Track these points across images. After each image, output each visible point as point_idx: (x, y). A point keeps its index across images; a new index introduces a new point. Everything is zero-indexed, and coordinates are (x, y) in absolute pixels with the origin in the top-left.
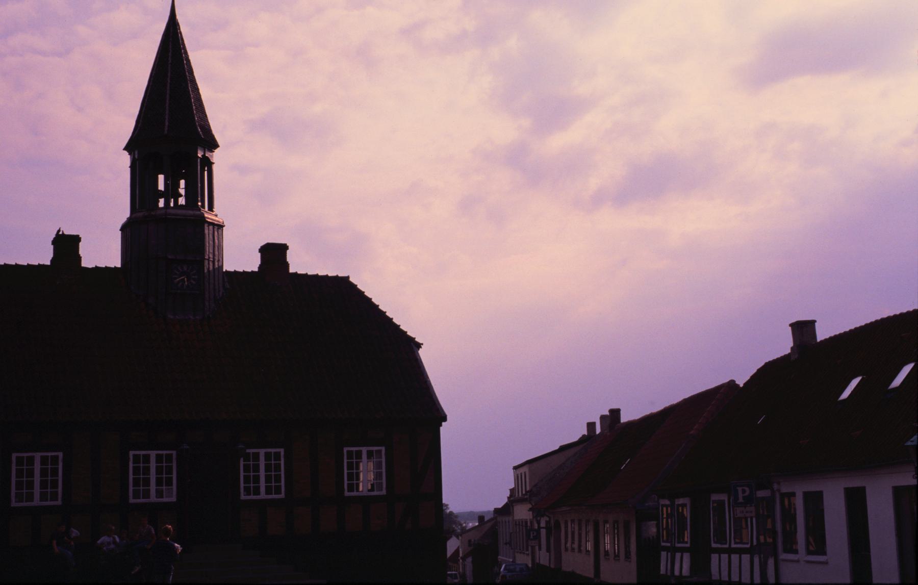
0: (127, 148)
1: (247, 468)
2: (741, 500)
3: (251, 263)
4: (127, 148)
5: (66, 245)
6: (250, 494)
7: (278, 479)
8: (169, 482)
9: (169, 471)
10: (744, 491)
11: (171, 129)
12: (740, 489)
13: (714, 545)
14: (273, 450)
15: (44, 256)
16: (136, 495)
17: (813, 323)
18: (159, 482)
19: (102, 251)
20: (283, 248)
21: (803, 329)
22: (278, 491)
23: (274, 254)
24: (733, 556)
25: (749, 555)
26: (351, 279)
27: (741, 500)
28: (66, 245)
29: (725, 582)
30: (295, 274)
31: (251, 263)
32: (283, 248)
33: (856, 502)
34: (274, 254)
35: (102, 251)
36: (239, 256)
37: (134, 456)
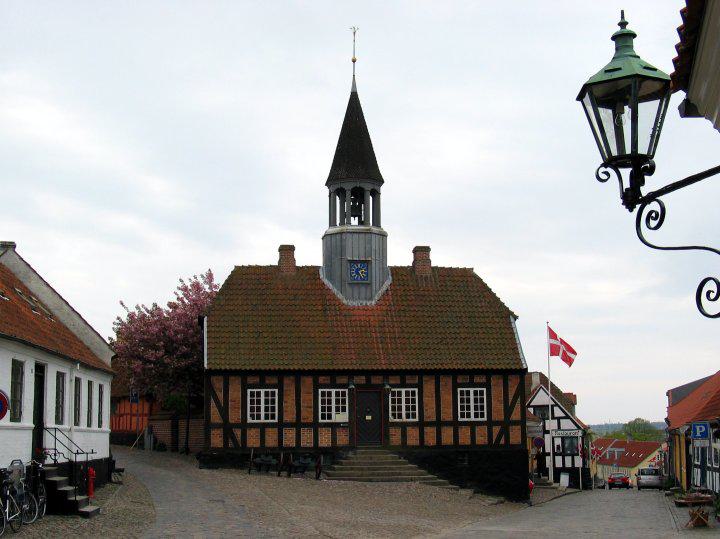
1: (393, 401)
2: (698, 434)
5: (287, 251)
7: (252, 402)
9: (344, 402)
10: (701, 429)
12: (698, 428)
14: (270, 390)
16: (462, 416)
19: (311, 255)
20: (426, 250)
23: (422, 253)
24: (566, 458)
25: (320, 445)
26: (474, 271)
27: (698, 434)
28: (287, 251)
30: (436, 268)
32: (426, 250)
34: (422, 253)
35: (311, 255)
36: (399, 255)
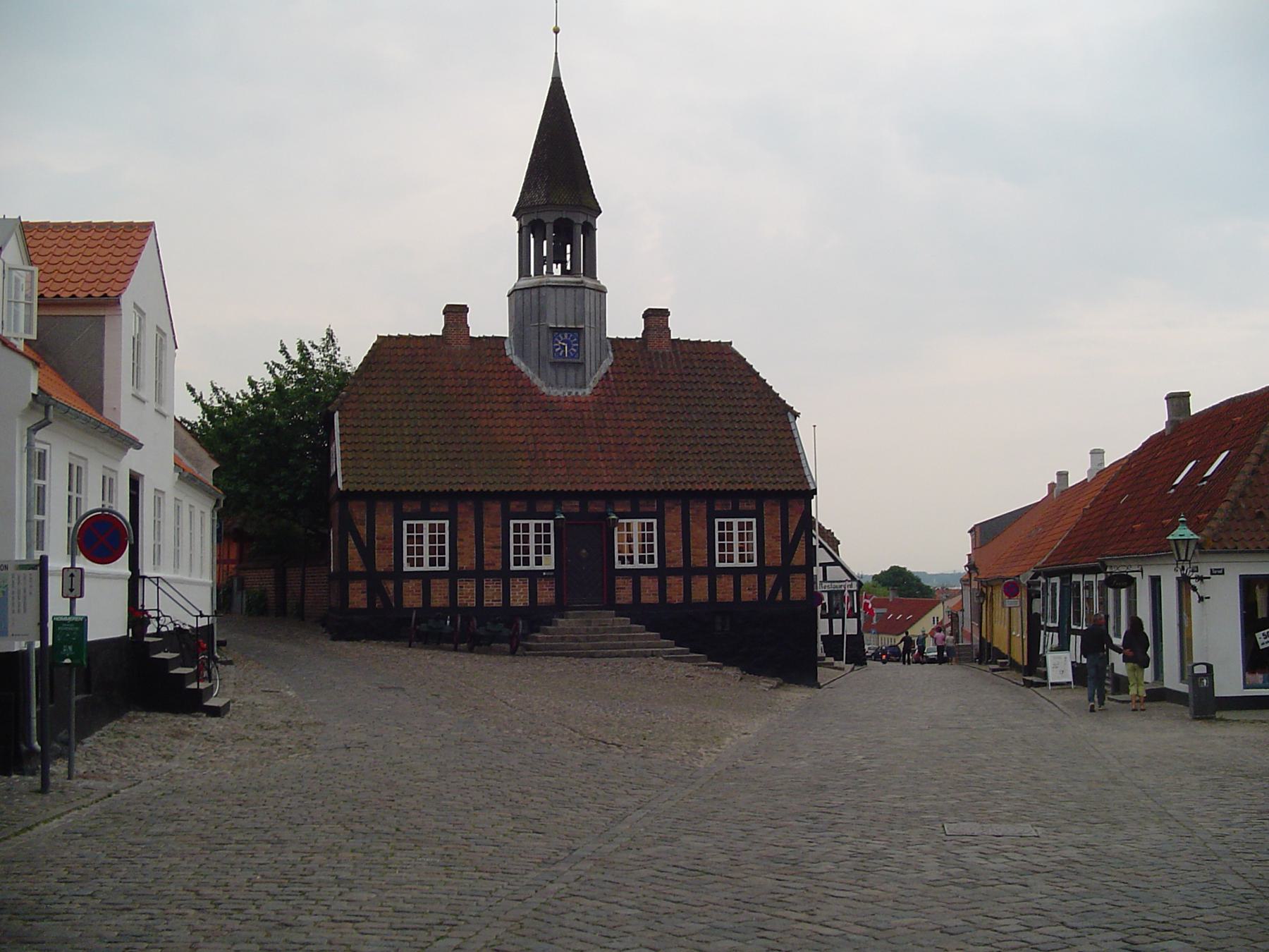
0: (514, 215)
3: (634, 329)
4: (514, 215)
5: (456, 314)
6: (412, 565)
8: (547, 551)
9: (547, 539)
11: (558, 194)
13: (1073, 627)
15: (434, 326)
17: (1187, 395)
18: (538, 550)
21: (1178, 401)
22: (442, 563)
23: (657, 318)
28: (456, 314)
29: (674, 606)
31: (634, 329)
32: (664, 313)
33: (1156, 582)
34: (657, 318)
36: (623, 322)
37: (515, 525)
